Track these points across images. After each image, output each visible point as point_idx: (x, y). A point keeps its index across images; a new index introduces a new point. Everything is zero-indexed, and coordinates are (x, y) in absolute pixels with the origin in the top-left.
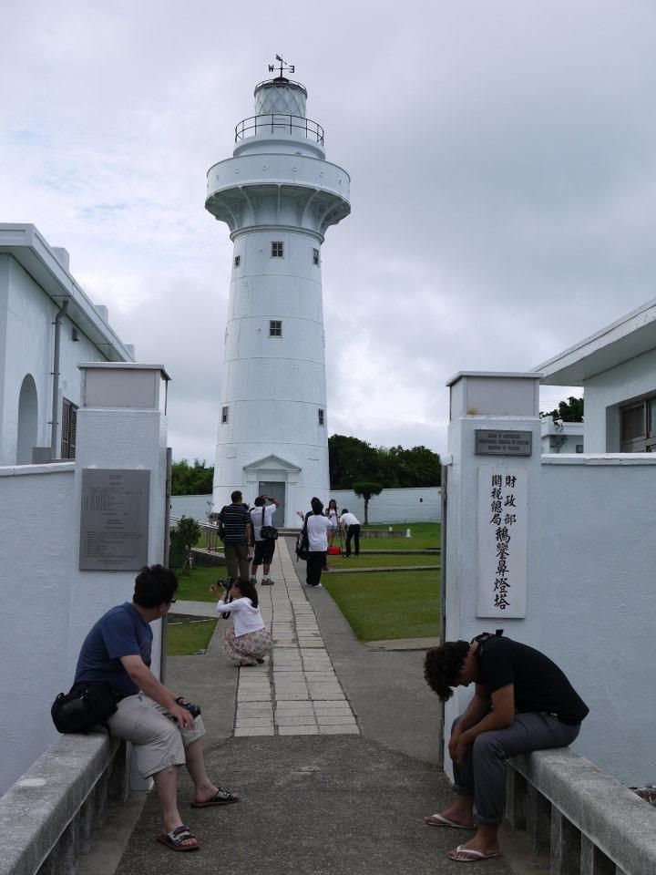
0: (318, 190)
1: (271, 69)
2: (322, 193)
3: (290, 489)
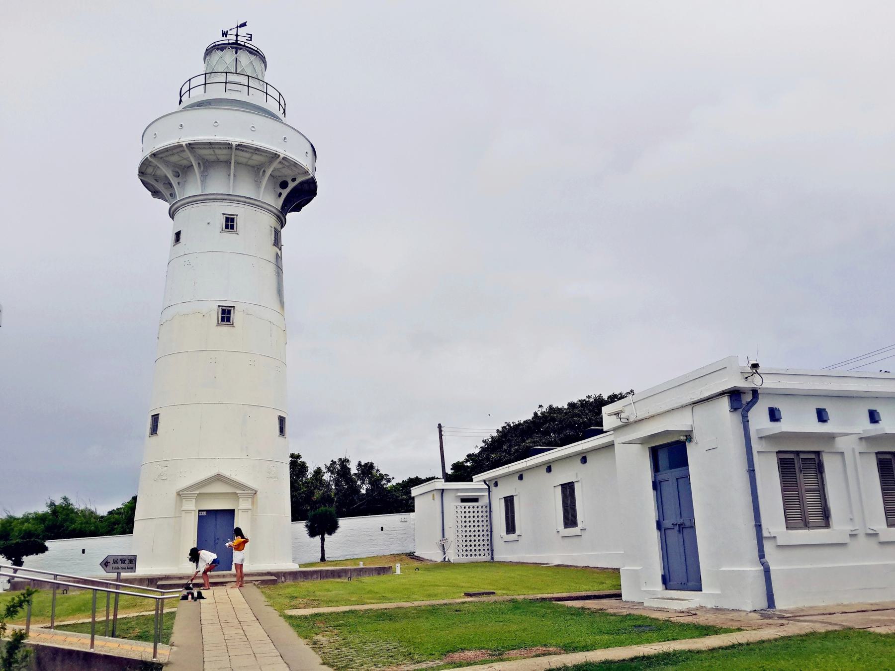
0: (282, 156)
1: (225, 34)
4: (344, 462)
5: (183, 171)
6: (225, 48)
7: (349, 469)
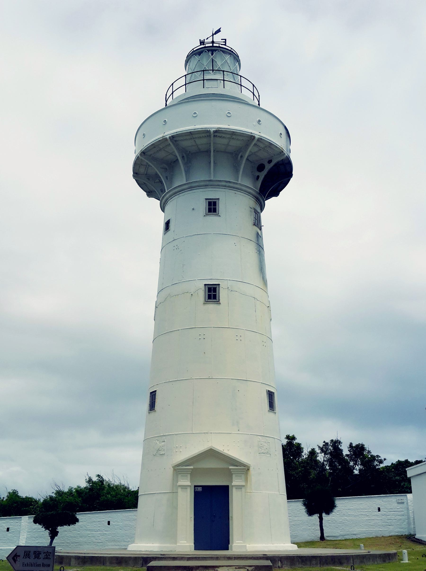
2: (260, 140)
3: (235, 497)
4: (336, 444)
5: (170, 166)
6: (202, 52)
7: (341, 451)
